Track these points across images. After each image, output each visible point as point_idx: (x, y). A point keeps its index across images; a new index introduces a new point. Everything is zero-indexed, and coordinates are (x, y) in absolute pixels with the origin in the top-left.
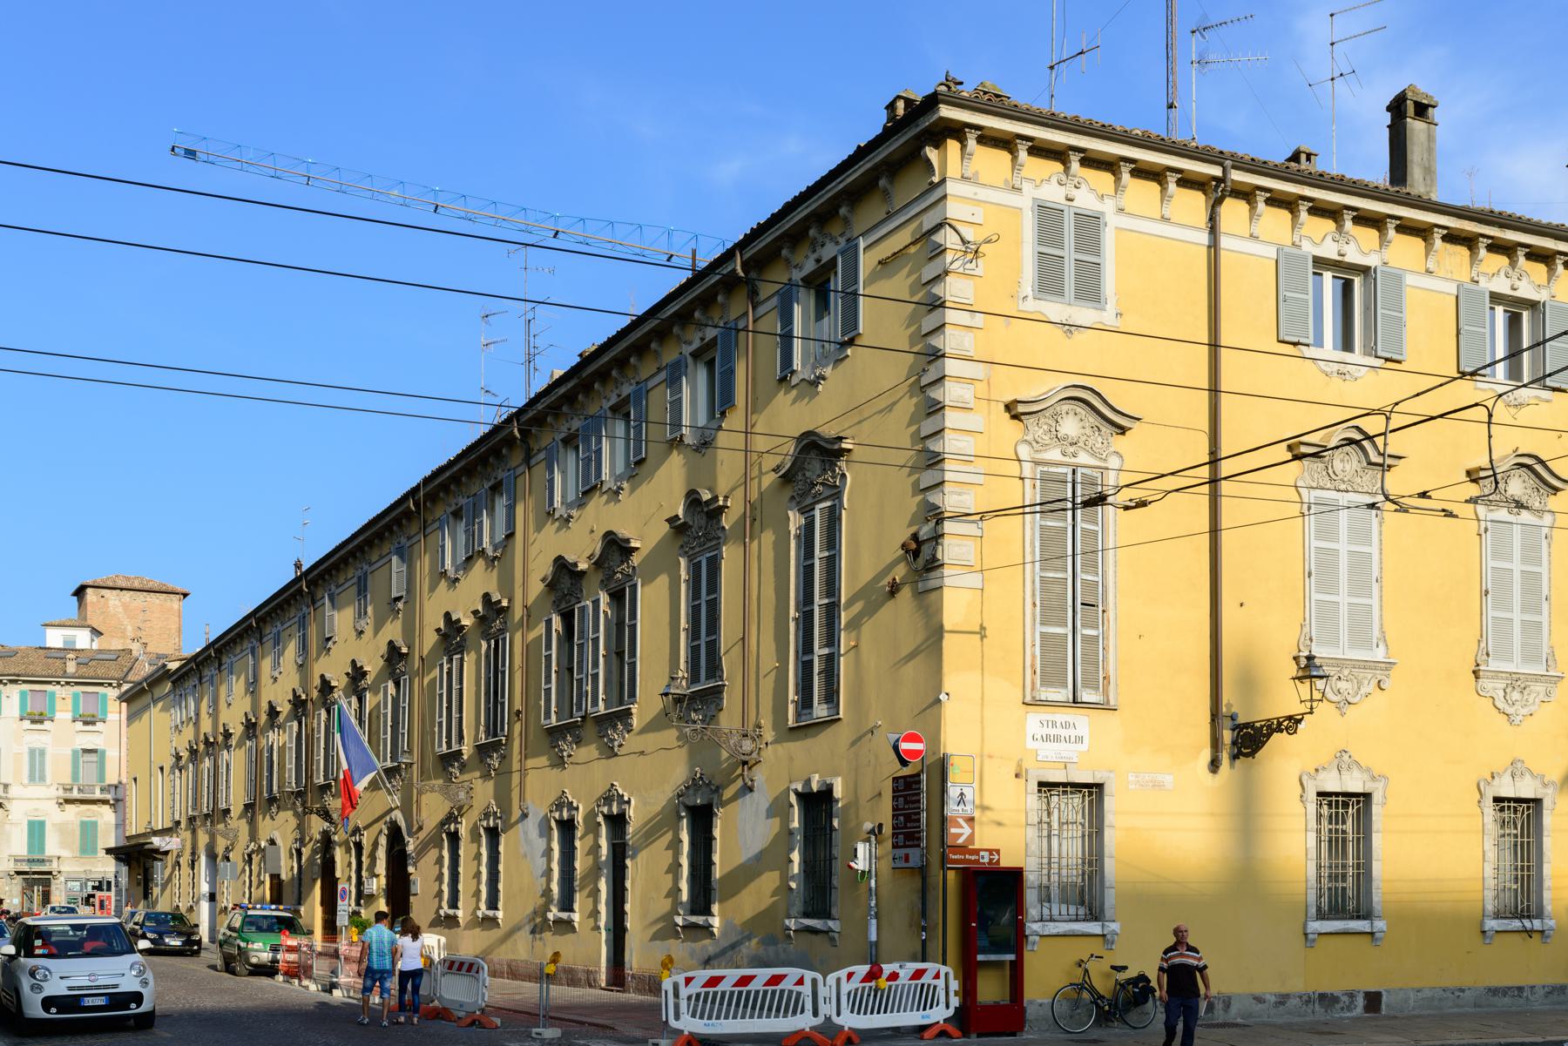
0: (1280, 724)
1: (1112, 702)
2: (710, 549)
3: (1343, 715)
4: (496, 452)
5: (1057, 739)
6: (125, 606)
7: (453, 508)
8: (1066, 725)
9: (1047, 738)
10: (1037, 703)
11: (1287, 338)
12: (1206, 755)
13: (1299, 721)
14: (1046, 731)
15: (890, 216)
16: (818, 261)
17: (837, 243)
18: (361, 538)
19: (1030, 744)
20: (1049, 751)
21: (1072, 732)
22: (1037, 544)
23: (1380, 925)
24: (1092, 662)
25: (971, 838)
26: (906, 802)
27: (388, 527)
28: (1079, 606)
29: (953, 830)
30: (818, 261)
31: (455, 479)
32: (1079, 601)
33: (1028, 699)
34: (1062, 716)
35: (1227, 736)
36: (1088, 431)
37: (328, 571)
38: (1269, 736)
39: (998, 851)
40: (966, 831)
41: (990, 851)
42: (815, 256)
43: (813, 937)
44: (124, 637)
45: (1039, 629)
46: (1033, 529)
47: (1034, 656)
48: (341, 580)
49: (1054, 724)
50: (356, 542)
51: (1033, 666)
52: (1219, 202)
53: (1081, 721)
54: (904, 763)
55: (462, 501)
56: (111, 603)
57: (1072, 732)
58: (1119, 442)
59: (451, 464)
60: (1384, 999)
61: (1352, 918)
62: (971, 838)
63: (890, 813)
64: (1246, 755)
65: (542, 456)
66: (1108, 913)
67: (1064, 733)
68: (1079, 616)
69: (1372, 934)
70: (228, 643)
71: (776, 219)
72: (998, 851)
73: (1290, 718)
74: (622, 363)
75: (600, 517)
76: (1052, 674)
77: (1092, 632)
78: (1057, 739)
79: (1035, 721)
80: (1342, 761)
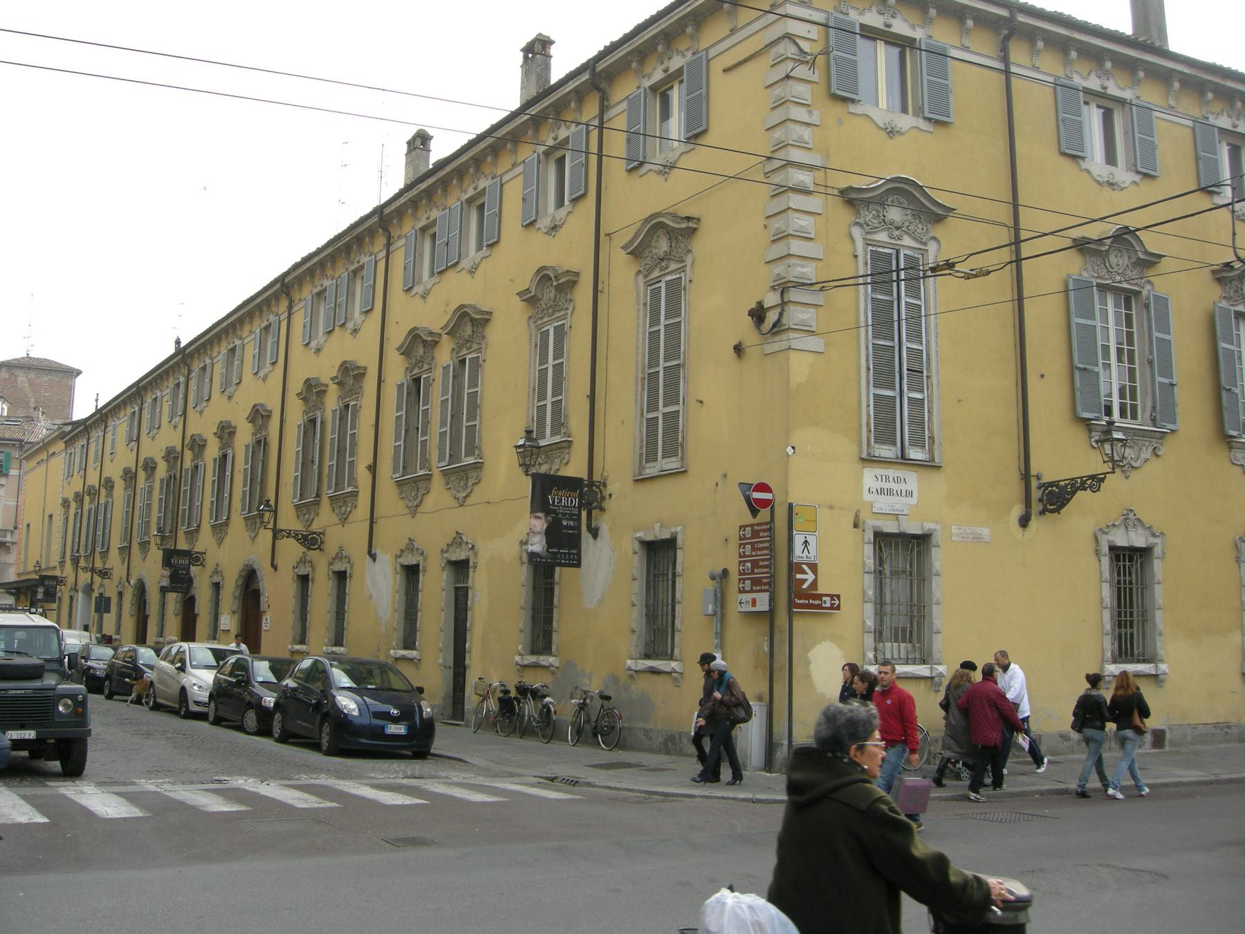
0: (1083, 483)
1: (937, 460)
2: (558, 319)
3: (1127, 477)
4: (359, 240)
5: (890, 492)
6: (31, 383)
7: (319, 289)
8: (897, 480)
9: (881, 492)
10: (870, 460)
11: (1068, 151)
12: (1017, 510)
13: (1102, 480)
14: (880, 485)
15: (733, 31)
16: (666, 71)
17: (684, 56)
18: (235, 317)
19: (867, 497)
20: (883, 504)
21: (903, 487)
22: (870, 315)
23: (1163, 667)
24: (918, 422)
25: (814, 584)
26: (753, 549)
27: (259, 307)
28: (905, 372)
29: (798, 576)
30: (666, 71)
31: (322, 264)
32: (905, 367)
33: (864, 455)
34: (892, 472)
35: (1036, 494)
36: (910, 217)
37: (204, 345)
38: (1073, 493)
39: (838, 597)
40: (810, 577)
41: (832, 596)
42: (663, 67)
43: (655, 677)
44: (28, 407)
45: (872, 391)
46: (866, 300)
47: (868, 416)
48: (215, 354)
49: (887, 478)
50: (230, 320)
51: (868, 424)
52: (1007, 38)
53: (911, 480)
54: (754, 512)
55: (327, 283)
56: (20, 379)
57: (903, 487)
58: (938, 231)
59: (319, 251)
60: (1168, 736)
61: (1139, 662)
62: (814, 584)
63: (736, 559)
64: (1052, 511)
65: (402, 242)
66: (936, 656)
67: (895, 487)
68: (905, 381)
69: (1156, 676)
70: (114, 408)
71: (627, 38)
72: (838, 597)
73: (1093, 477)
74: (478, 162)
75: (457, 290)
76: (884, 430)
77: (918, 396)
78: (890, 492)
79: (870, 477)
80: (1129, 519)
